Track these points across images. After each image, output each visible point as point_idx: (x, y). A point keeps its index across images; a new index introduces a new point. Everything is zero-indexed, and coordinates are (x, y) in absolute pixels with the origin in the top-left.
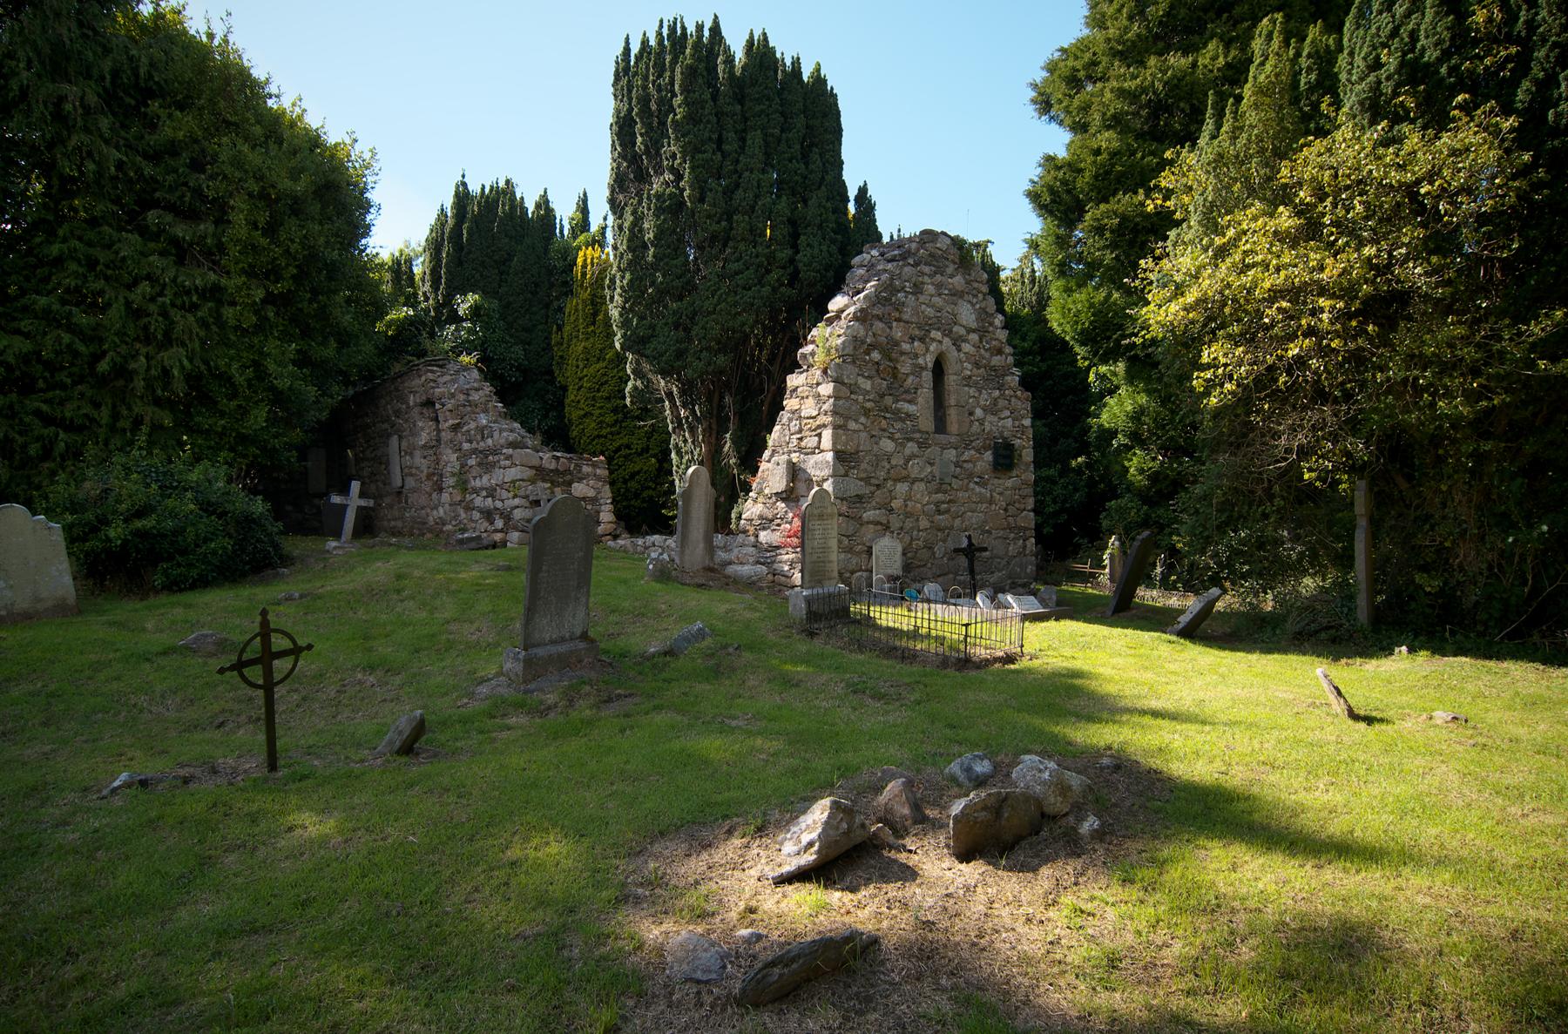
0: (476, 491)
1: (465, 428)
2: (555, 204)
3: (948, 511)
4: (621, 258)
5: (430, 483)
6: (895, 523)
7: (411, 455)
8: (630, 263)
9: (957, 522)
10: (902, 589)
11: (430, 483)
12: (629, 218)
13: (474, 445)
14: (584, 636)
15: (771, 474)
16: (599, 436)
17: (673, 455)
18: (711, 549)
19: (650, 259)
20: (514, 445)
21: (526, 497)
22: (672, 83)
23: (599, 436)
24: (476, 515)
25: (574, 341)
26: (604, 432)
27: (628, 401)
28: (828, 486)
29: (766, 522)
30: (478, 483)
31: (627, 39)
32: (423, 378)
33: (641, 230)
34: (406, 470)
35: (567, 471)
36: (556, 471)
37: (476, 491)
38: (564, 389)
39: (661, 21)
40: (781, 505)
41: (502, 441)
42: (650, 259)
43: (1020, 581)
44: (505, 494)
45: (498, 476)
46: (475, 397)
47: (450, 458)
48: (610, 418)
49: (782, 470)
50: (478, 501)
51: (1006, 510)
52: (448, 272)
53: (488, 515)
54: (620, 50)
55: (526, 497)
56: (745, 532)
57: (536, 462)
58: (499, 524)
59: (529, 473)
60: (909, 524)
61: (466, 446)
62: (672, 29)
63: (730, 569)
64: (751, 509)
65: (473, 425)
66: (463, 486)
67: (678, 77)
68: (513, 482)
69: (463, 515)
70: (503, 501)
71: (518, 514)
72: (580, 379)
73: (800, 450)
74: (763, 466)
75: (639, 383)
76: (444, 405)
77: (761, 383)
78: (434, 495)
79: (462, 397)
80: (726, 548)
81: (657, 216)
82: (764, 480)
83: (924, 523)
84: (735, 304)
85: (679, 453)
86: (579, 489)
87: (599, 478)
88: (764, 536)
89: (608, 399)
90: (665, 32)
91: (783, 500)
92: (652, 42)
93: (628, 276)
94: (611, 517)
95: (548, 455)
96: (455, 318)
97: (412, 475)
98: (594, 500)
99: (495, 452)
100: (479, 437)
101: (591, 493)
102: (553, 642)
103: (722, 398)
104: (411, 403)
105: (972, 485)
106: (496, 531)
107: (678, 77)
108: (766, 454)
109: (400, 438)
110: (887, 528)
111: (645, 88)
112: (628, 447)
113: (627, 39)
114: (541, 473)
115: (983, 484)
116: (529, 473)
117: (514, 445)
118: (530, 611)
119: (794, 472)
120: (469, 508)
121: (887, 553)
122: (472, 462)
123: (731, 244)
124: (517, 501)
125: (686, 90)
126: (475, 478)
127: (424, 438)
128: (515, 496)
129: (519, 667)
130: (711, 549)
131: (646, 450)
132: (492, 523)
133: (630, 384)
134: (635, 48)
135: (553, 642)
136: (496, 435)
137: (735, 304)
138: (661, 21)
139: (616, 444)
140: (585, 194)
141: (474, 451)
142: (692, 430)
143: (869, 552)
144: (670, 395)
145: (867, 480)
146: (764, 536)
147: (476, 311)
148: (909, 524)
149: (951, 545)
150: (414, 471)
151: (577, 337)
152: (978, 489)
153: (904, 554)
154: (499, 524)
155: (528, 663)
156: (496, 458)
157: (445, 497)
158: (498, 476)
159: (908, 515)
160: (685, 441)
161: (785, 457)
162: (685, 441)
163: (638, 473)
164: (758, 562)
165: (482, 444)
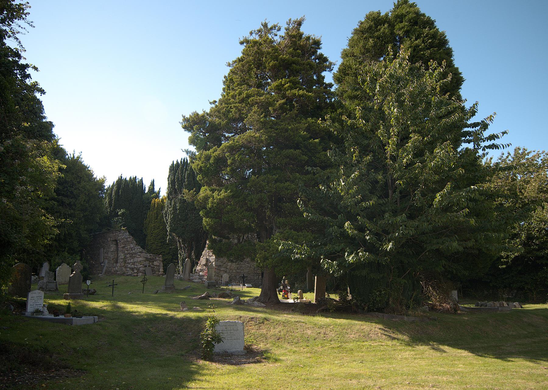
0: (129, 263)
1: (126, 247)
2: (144, 182)
3: (240, 269)
4: (171, 211)
5: (113, 261)
6: (228, 271)
7: (107, 253)
8: (173, 213)
9: (242, 271)
10: (227, 284)
11: (113, 261)
12: (173, 203)
13: (129, 252)
14: (173, 285)
15: (203, 260)
16: (156, 249)
17: (179, 255)
18: (190, 276)
19: (178, 212)
20: (141, 252)
21: (143, 265)
22: (185, 175)
23: (156, 249)
24: (128, 269)
25: (151, 223)
26: (158, 248)
27: (167, 241)
28: (214, 263)
29: (201, 270)
30: (129, 261)
31: (173, 161)
32: (114, 234)
33: (176, 206)
34: (105, 257)
35: (153, 259)
36: (150, 259)
37: (129, 263)
38: (146, 236)
39: (182, 159)
40: (204, 267)
41: (138, 251)
42: (178, 212)
43: (257, 285)
44: (138, 264)
45: (136, 260)
46: (129, 240)
47: (122, 255)
48: (160, 244)
49: (205, 260)
50: (129, 266)
51: (254, 269)
52: (115, 202)
53: (132, 269)
54: (172, 163)
55: (143, 265)
56: (197, 272)
57: (146, 257)
58: (136, 271)
59: (145, 259)
60: (231, 271)
61: (126, 252)
62: (184, 160)
63: (193, 280)
64: (198, 268)
65: (129, 247)
66: (125, 262)
67: (186, 175)
68: (140, 261)
69: (124, 269)
70: (137, 266)
71: (141, 269)
72: (152, 234)
73: (209, 256)
74: (201, 259)
75: (170, 237)
76: (120, 241)
77: (201, 239)
78: (115, 264)
79: (126, 240)
80: (192, 276)
81: (180, 203)
82: (201, 262)
83: (234, 271)
84: (196, 223)
85: (181, 255)
86: (155, 263)
87: (160, 260)
88: (201, 273)
89: (160, 239)
90: (182, 161)
91: (205, 266)
92: (179, 162)
93: (172, 216)
94: (163, 270)
95: (149, 255)
96: (117, 215)
97: (107, 259)
98: (159, 266)
99: (135, 254)
100: (131, 250)
101: (158, 264)
102: (169, 285)
103: (192, 242)
104: (109, 240)
105: (246, 264)
106: (135, 273)
107: (186, 175)
108: (202, 256)
109: (104, 249)
110: (226, 272)
111: (178, 175)
112: (164, 252)
113: (173, 161)
114: (147, 259)
115: (248, 263)
116: (145, 259)
117: (141, 252)
118: (166, 281)
119: (207, 260)
120: (126, 267)
121: (226, 277)
122: (128, 256)
123: (196, 210)
124: (141, 266)
125: (188, 178)
126: (128, 260)
127: (112, 249)
128: (141, 265)
129: (165, 288)
130: (190, 276)
131: (169, 253)
132: (133, 271)
133: (168, 237)
134: (175, 163)
135: (169, 285)
136: (136, 250)
137: (196, 223)
138: (182, 159)
139: (161, 251)
140: (154, 181)
141: (129, 253)
142: (184, 250)
143: (222, 276)
144: (179, 242)
145: (222, 262)
146: (201, 273)
147: (123, 214)
148: (231, 271)
149: (240, 276)
150: (108, 258)
151: (152, 222)
152: (247, 264)
153: (229, 277)
154: (136, 271)
155: (166, 287)
156: (136, 255)
157: (118, 265)
158: (136, 260)
159: (231, 269)
160: (182, 252)
161: (206, 257)
162: (182, 252)
163: (166, 259)
164: (199, 279)
165: (131, 252)
